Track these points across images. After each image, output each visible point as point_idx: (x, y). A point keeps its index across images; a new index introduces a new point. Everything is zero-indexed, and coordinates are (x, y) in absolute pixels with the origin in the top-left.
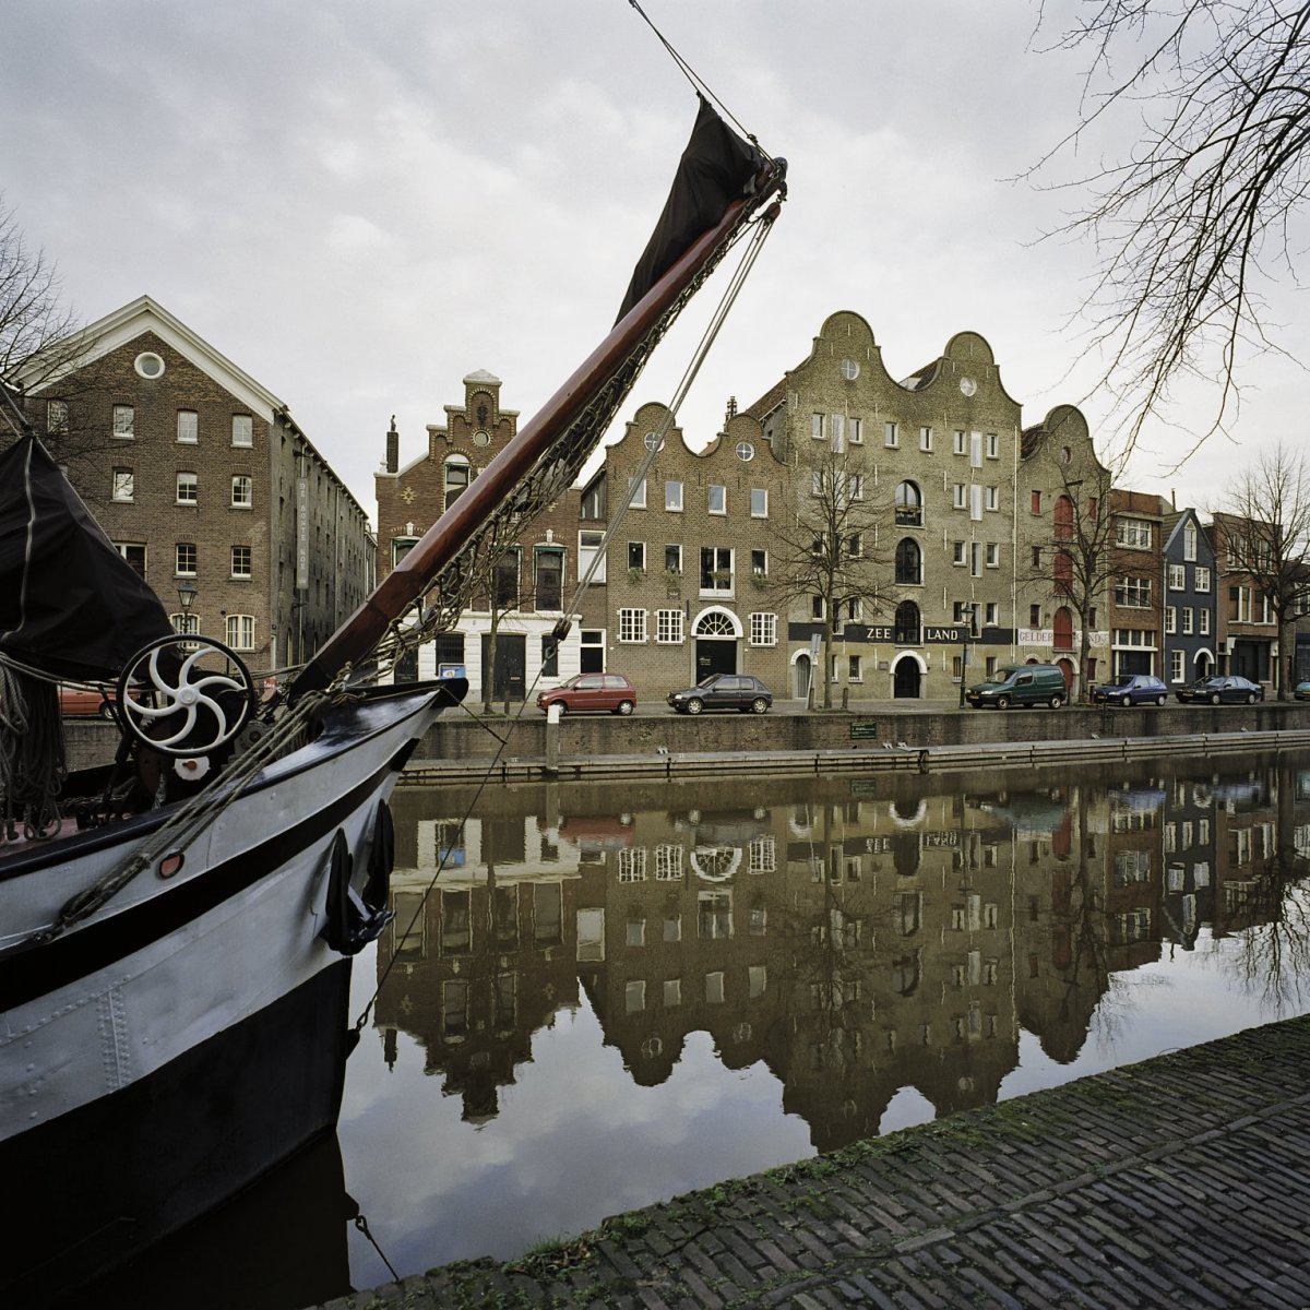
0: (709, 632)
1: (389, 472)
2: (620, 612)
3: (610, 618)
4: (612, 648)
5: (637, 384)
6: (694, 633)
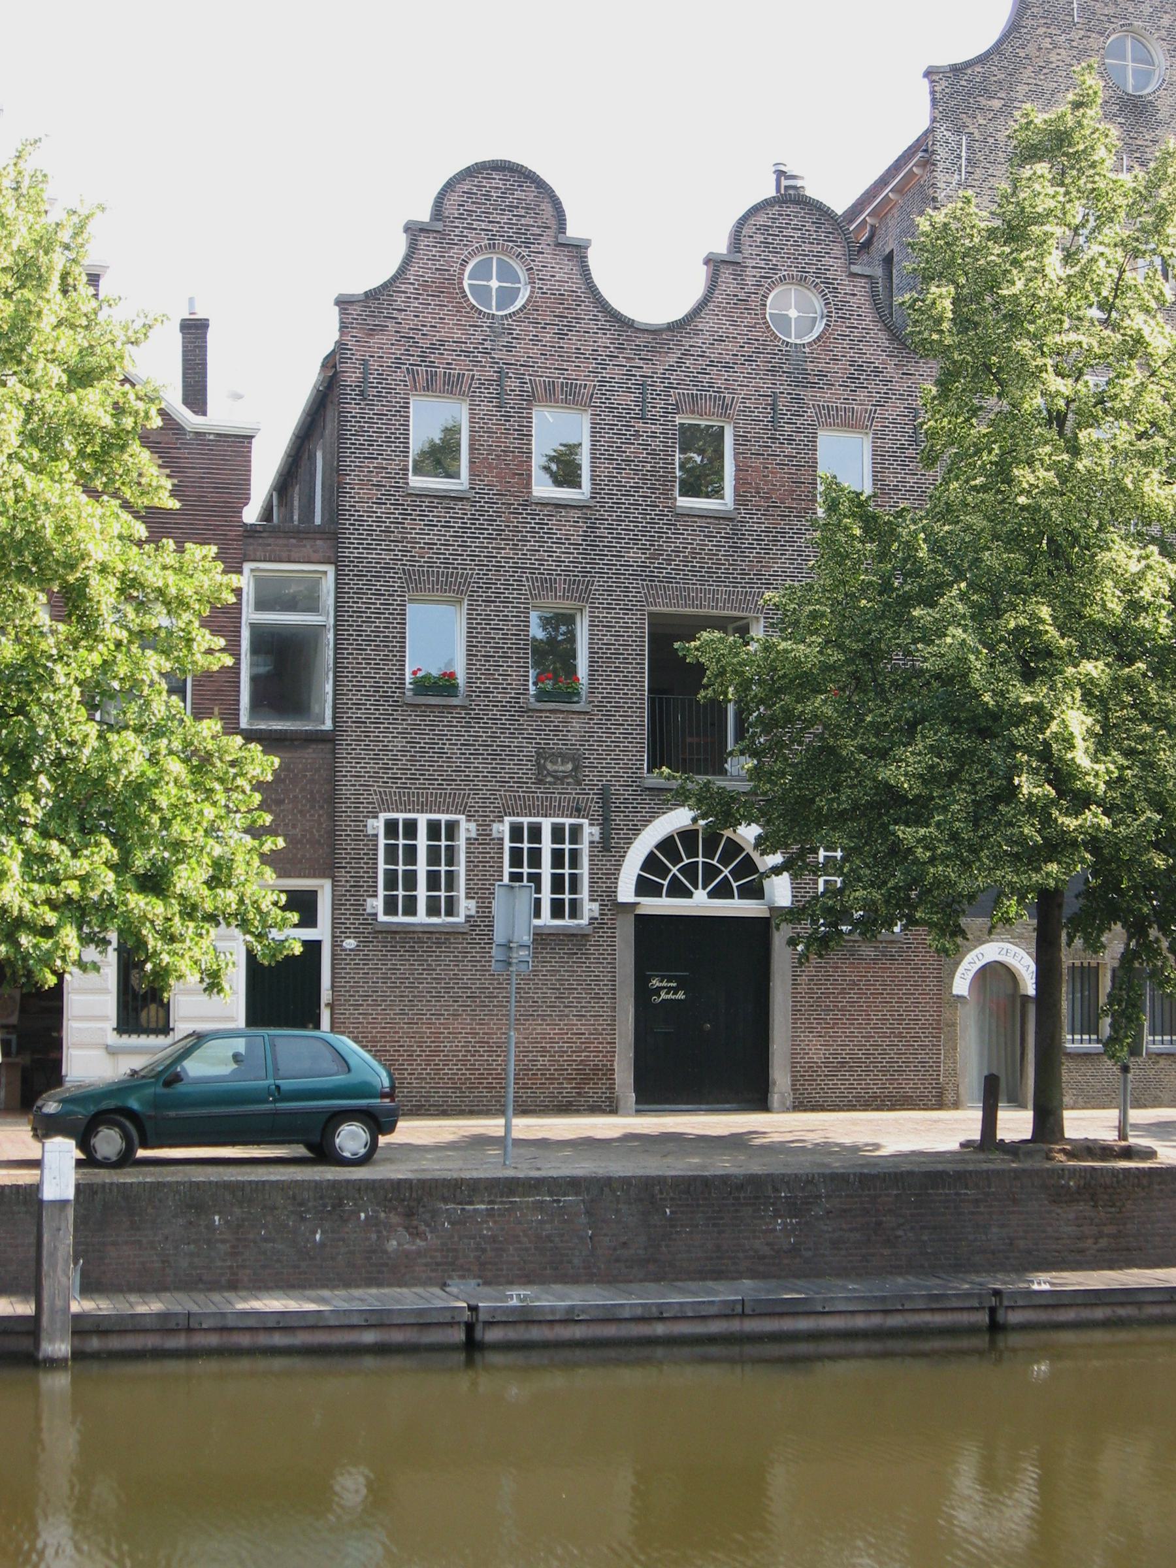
0: (679, 890)
1: (540, 824)
2: (377, 826)
3: (347, 845)
4: (350, 943)
5: (567, 217)
6: (626, 892)
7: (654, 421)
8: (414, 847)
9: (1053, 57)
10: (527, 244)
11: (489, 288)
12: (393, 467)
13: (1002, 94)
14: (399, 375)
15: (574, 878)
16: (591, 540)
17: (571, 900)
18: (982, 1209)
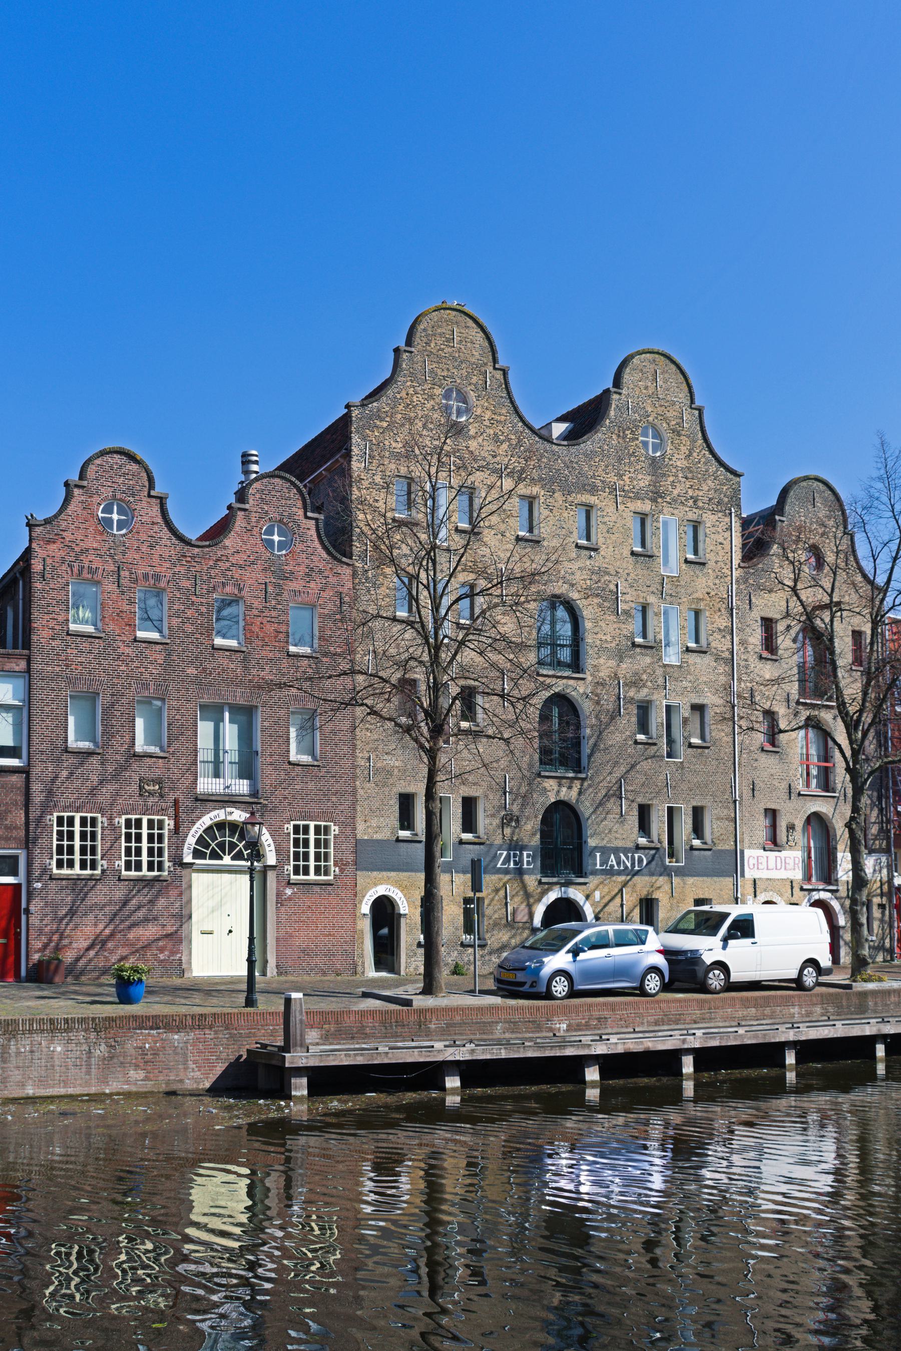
7: (202, 596)
8: (73, 832)
9: (415, 399)
10: (133, 495)
11: (273, 541)
12: (61, 618)
13: (388, 419)
14: (64, 567)
15: (326, 854)
16: (168, 662)
17: (325, 866)
18: (220, 1036)
